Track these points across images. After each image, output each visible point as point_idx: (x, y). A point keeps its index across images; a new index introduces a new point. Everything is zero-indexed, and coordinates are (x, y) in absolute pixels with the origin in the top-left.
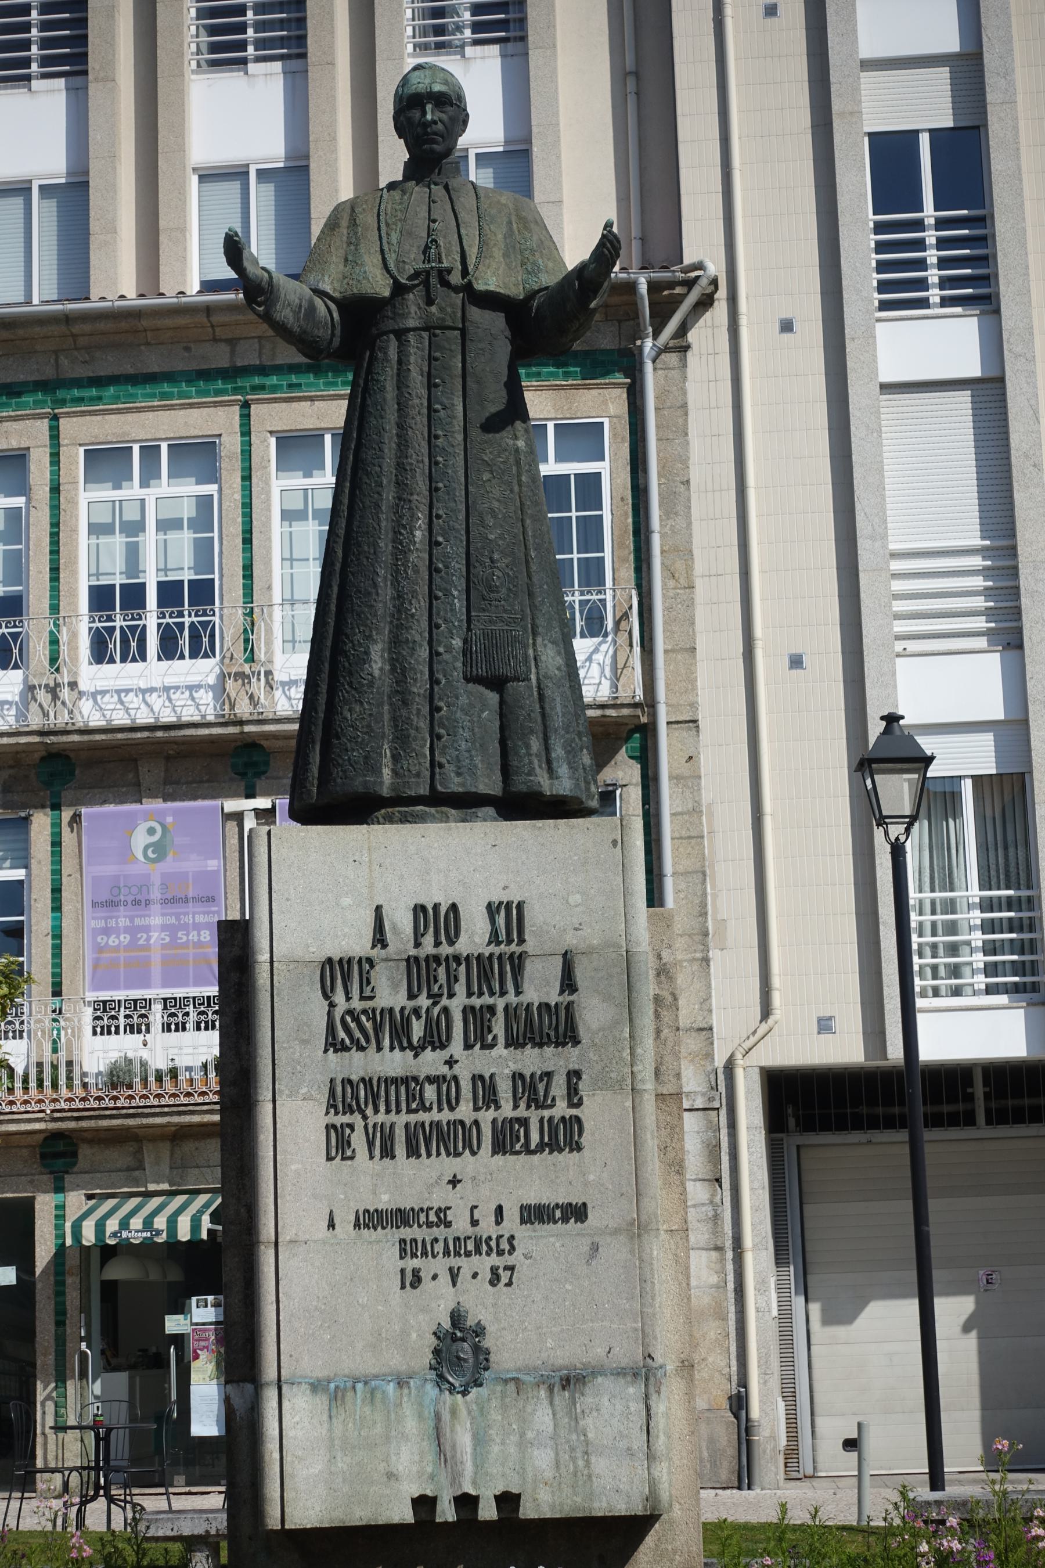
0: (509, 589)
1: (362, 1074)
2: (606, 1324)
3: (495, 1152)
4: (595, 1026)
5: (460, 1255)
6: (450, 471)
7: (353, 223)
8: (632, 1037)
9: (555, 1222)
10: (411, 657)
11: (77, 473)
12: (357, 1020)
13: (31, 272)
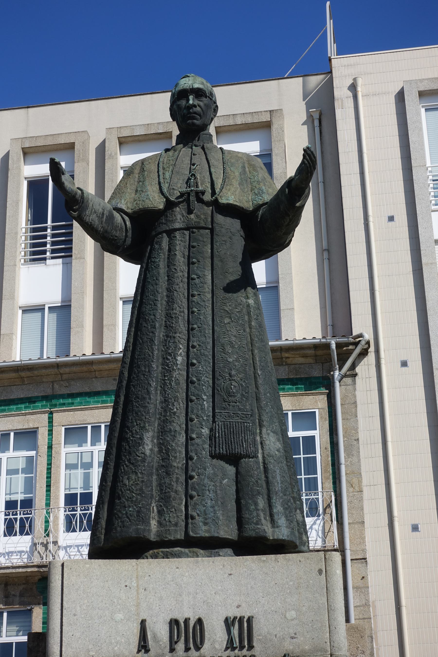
0: (242, 395)
6: (202, 317)
7: (142, 170)
10: (173, 441)
11: (61, 439)
13: (43, 346)
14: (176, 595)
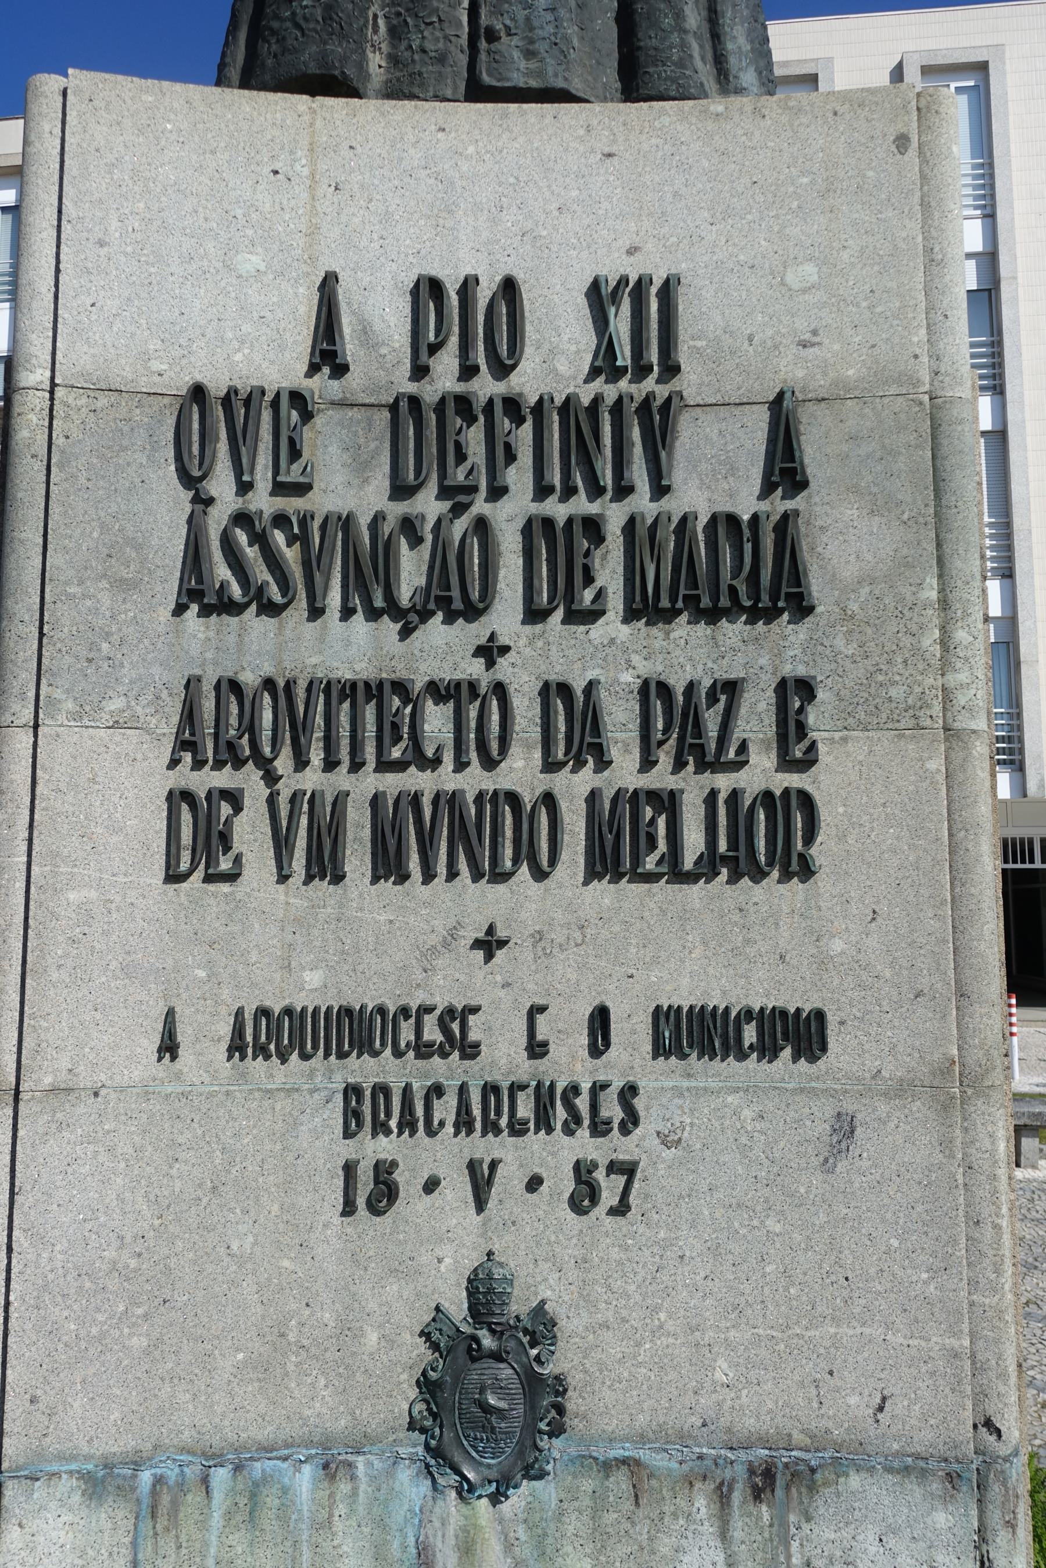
1: (268, 669)
2: (876, 1331)
3: (592, 874)
4: (849, 572)
5: (497, 1131)
8: (944, 604)
9: (742, 1056)
12: (260, 539)
14: (436, 211)
